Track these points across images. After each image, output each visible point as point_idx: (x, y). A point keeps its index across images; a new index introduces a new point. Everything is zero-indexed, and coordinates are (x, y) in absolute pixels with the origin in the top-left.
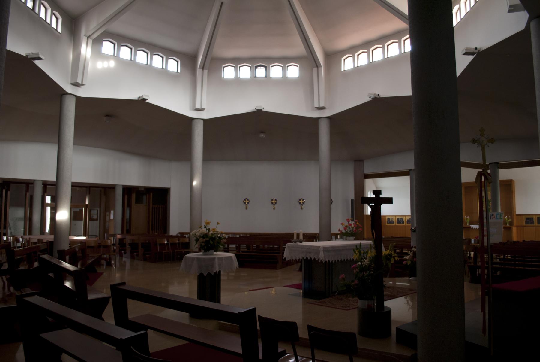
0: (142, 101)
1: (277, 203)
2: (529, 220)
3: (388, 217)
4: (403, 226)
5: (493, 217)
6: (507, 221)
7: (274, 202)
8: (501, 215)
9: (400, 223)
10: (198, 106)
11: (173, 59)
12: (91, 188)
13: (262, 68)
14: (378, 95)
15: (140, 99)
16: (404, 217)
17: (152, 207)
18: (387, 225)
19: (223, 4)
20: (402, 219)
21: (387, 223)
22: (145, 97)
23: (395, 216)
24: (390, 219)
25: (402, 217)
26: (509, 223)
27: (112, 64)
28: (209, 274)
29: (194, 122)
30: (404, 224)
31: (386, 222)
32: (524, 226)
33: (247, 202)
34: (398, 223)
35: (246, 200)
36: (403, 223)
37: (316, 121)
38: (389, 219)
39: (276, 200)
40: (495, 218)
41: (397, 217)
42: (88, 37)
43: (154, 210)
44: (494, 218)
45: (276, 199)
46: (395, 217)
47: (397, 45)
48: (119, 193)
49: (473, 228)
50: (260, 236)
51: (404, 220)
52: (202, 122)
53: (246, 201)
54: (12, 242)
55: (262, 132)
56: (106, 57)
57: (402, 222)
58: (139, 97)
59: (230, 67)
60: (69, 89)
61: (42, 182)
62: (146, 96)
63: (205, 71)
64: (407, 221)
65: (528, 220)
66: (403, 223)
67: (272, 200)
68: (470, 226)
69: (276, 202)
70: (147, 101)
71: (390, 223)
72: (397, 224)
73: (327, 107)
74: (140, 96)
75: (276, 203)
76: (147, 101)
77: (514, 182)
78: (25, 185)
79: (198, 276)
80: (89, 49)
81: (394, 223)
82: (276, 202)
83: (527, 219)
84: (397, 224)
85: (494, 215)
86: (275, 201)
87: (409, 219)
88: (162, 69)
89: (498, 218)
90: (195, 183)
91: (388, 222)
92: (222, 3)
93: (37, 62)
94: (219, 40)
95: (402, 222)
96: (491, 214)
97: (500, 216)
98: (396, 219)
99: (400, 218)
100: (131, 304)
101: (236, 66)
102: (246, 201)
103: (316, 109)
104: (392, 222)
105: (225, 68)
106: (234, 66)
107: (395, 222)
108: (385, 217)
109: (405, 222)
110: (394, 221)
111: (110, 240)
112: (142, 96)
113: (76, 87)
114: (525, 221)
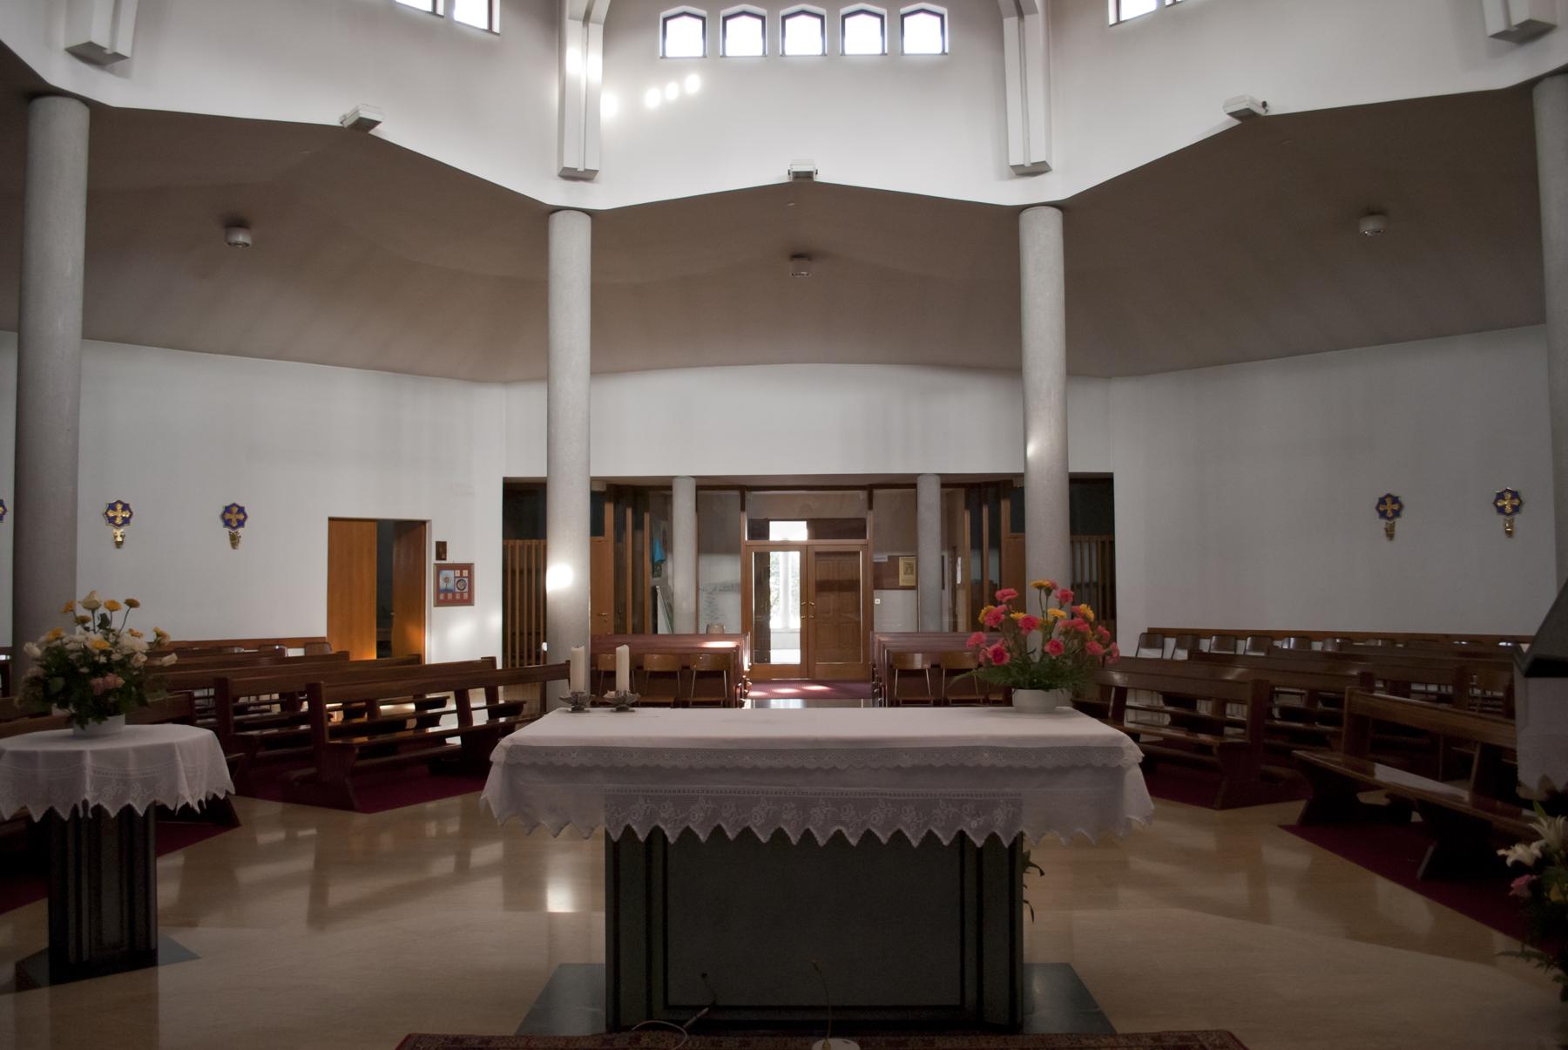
0: (803, 179)
1: (1524, 509)
7: (1507, 503)
10: (571, 162)
11: (803, 12)
12: (877, 492)
14: (1264, 104)
27: (693, 83)
28: (160, 811)
29: (558, 223)
33: (1505, 506)
35: (1388, 501)
37: (1013, 214)
39: (1515, 495)
42: (587, 18)
43: (509, 553)
45: (1514, 490)
48: (930, 500)
50: (390, 668)
52: (1054, 218)
53: (1389, 508)
54: (393, 658)
55: (1371, 213)
56: (679, 67)
61: (693, 483)
67: (1500, 496)
69: (1516, 502)
70: (372, 132)
73: (1558, 21)
75: (1516, 509)
76: (372, 132)
78: (736, 493)
80: (596, 57)
82: (1516, 502)
86: (1512, 498)
90: (1032, 449)
93: (1024, 888)
102: (1389, 508)
103: (1492, 39)
111: (1104, 658)
113: (581, 184)
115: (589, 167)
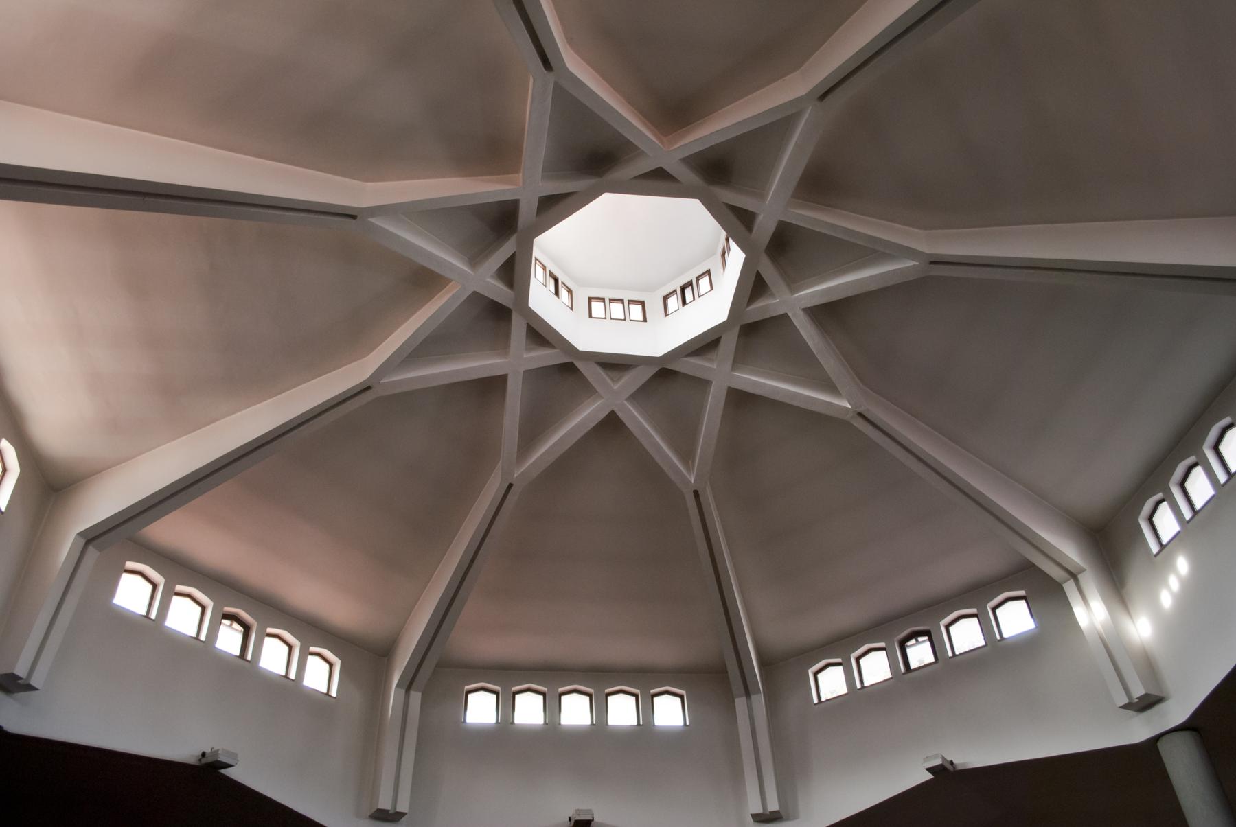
10: (385, 803)
13: (236, 626)
15: (204, 761)
19: (513, 488)
22: (222, 759)
47: (839, 671)
58: (203, 754)
59: (188, 600)
60: (1137, 731)
62: (228, 753)
63: (412, 693)
70: (223, 771)
74: (208, 750)
76: (223, 771)
79: (661, 168)
88: (639, 727)
92: (511, 485)
94: (472, 608)
100: (707, 278)
101: (1164, 493)
105: (862, 661)
106: (974, 611)
112: (215, 753)
115: (398, 810)
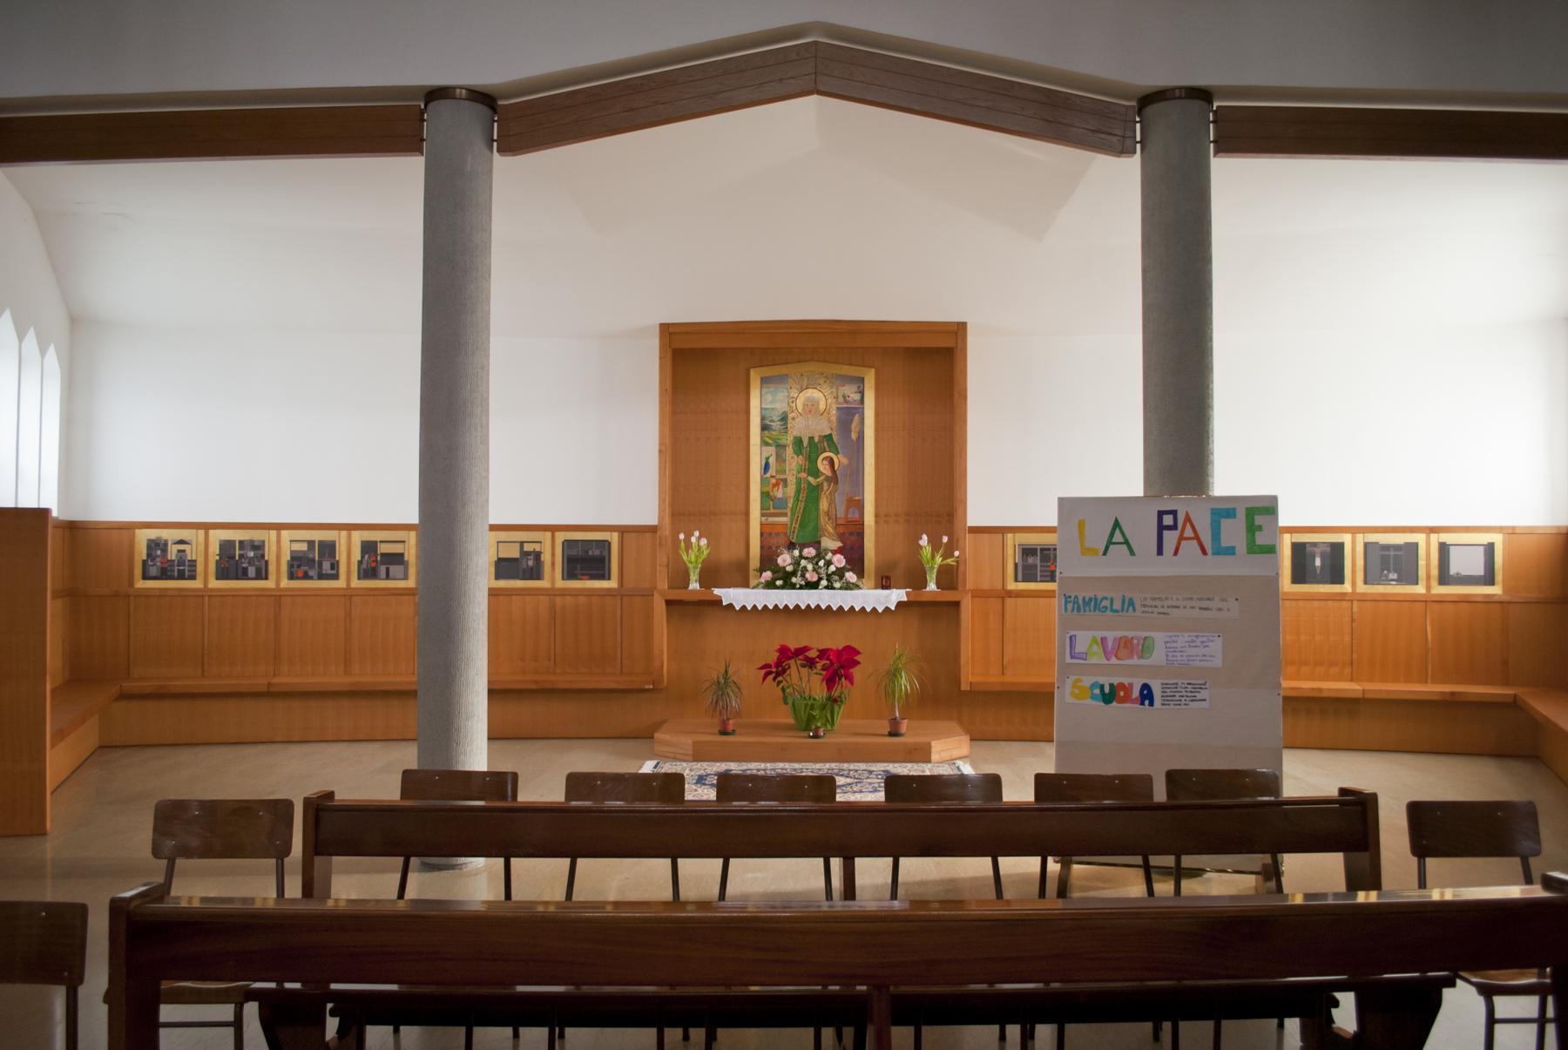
2: (1035, 560)
3: (153, 534)
4: (262, 593)
5: (1181, 538)
6: (927, 566)
8: (1259, 520)
9: (244, 575)
16: (273, 533)
17: (1191, 692)
18: (146, 595)
20: (258, 547)
21: (145, 577)
23: (207, 527)
24: (164, 549)
25: (256, 535)
26: (939, 572)
30: (269, 584)
31: (138, 571)
32: (1010, 594)
34: (222, 574)
36: (262, 574)
38: (156, 546)
40: (1204, 552)
41: (217, 536)
44: (1190, 547)
46: (201, 532)
49: (731, 606)
51: (270, 554)
57: (252, 571)
64: (291, 566)
65: (1030, 560)
66: (262, 574)
68: (717, 591)
71: (165, 574)
72: (214, 584)
77: (1132, 157)
81: (193, 577)
83: (1027, 551)
84: (214, 584)
85: (1188, 519)
87: (304, 547)
89: (1225, 542)
91: (153, 571)
95: (252, 571)
96: (1161, 514)
97: (1252, 529)
98: (214, 549)
99: (241, 542)
104: (185, 569)
107: (200, 568)
108: (133, 537)
109: (272, 568)
110: (193, 563)
114: (1016, 565)
